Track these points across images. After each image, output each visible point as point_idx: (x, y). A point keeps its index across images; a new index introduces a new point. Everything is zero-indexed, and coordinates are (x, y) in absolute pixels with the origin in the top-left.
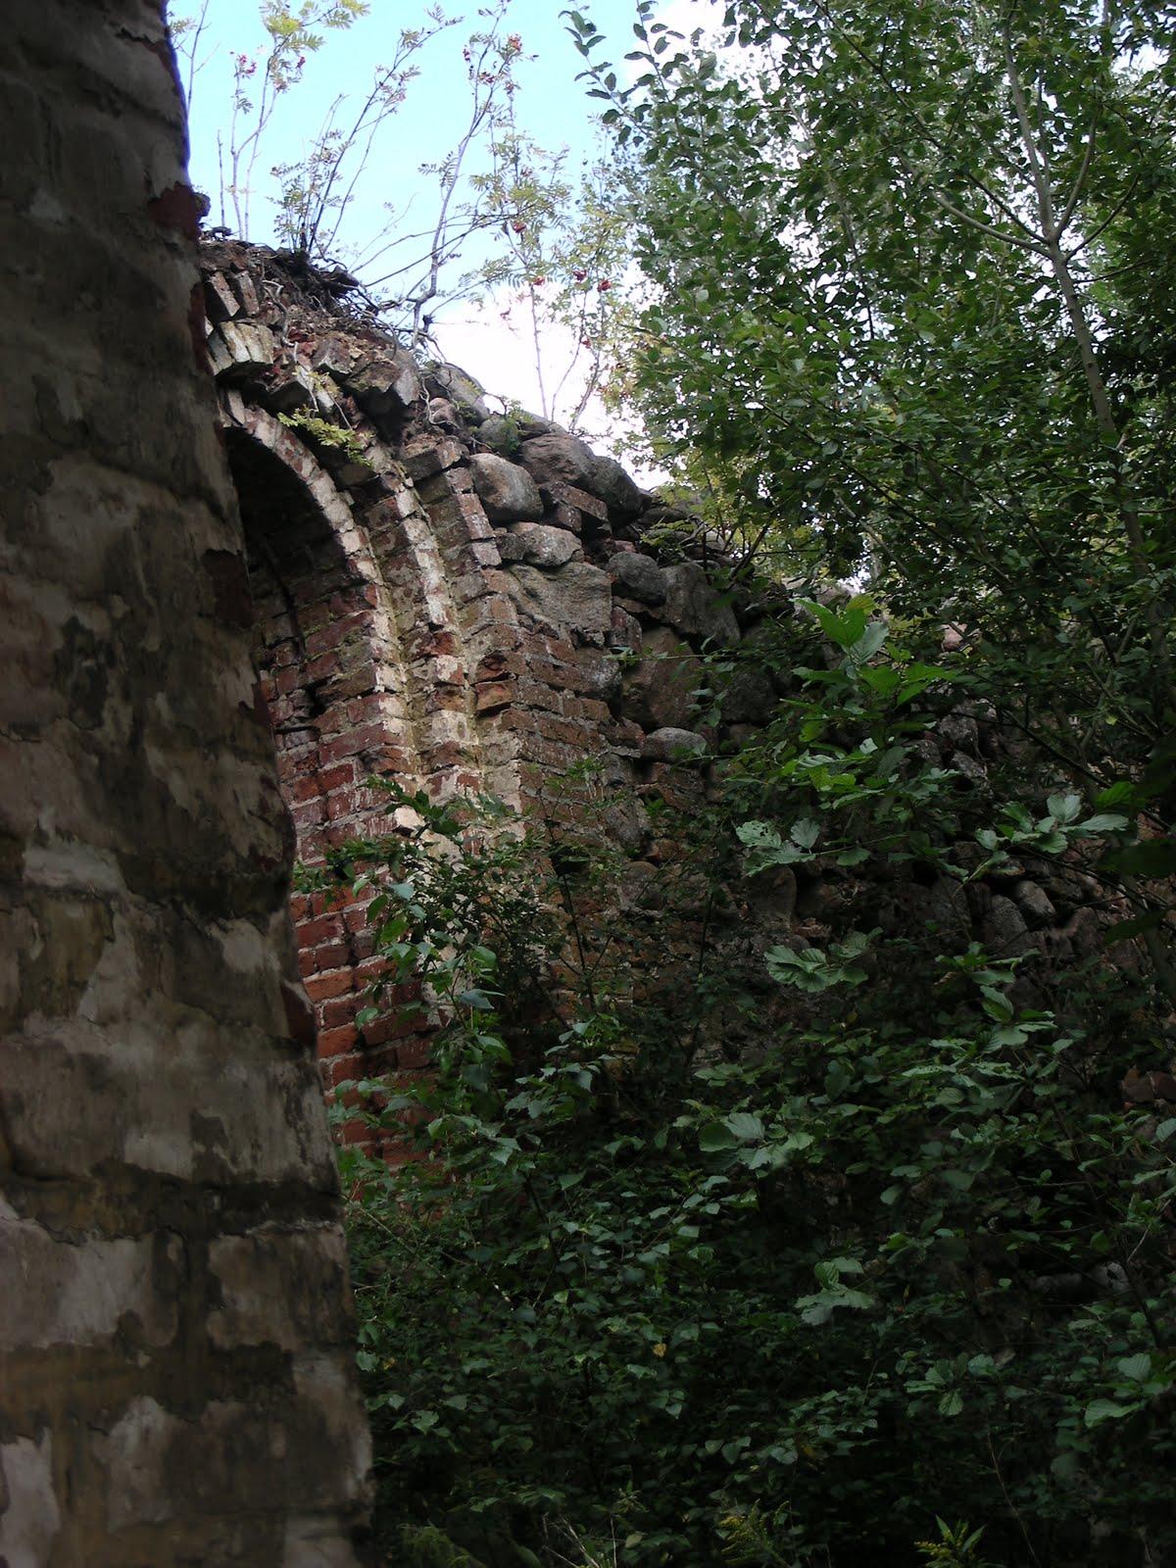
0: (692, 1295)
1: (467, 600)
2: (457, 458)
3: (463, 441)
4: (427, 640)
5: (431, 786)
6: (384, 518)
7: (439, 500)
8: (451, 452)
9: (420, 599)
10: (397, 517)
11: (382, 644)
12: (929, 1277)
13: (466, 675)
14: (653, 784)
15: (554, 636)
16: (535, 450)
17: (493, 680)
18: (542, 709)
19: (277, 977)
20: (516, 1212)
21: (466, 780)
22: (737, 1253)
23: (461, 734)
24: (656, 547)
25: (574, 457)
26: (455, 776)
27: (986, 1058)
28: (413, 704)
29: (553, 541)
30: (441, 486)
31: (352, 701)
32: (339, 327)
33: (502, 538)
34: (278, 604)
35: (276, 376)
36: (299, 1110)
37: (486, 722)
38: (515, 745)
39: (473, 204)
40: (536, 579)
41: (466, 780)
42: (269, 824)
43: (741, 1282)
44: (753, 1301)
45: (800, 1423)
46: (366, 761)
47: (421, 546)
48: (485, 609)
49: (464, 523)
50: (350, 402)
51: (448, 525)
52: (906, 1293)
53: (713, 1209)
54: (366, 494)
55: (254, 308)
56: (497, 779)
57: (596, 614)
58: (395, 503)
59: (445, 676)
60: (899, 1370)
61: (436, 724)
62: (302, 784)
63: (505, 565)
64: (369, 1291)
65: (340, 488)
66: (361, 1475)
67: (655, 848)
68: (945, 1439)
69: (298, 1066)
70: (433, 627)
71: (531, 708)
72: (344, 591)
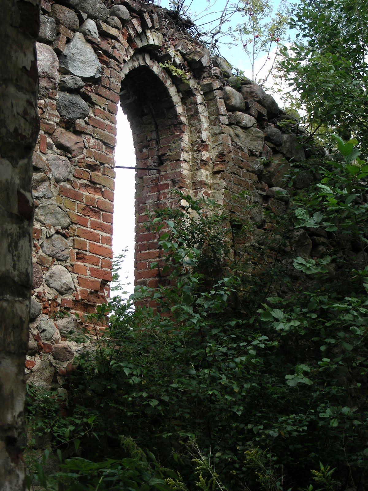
0: (254, 374)
1: (215, 134)
2: (219, 87)
3: (222, 82)
4: (200, 145)
5: (194, 194)
6: (191, 103)
7: (211, 100)
8: (217, 84)
9: (200, 132)
10: (196, 103)
11: (185, 145)
12: (334, 380)
13: (211, 159)
14: (269, 204)
15: (243, 150)
16: (246, 89)
17: (220, 162)
18: (235, 174)
19: (16, 187)
20: (199, 336)
21: (206, 193)
22: (271, 362)
23: (207, 178)
24: (282, 127)
25: (258, 92)
26: (203, 192)
27: (364, 307)
28: (192, 166)
29: (247, 119)
30: (212, 95)
31: (172, 162)
32: (186, 38)
33: (230, 115)
34: (153, 128)
35: (162, 51)
36: (16, 247)
37: (216, 175)
38: (224, 184)
39: (237, 4)
40: (239, 131)
41: (206, 193)
42: (27, 120)
43: (271, 372)
44: (273, 379)
45: (282, 423)
46: (174, 183)
47: (203, 114)
48: (221, 138)
49: (218, 109)
50: (186, 63)
51: (212, 109)
52: (325, 384)
53: (262, 346)
54: (187, 95)
55: (157, 26)
56: (216, 195)
57: (258, 146)
58: (196, 99)
59: (204, 158)
60: (318, 410)
61: (199, 174)
62: (152, 187)
63: (230, 125)
64: (147, 356)
65: (178, 91)
66: (16, 414)
67: (266, 226)
68: (331, 435)
69: (20, 227)
70: (202, 141)
71: (231, 173)
72: (175, 126)
